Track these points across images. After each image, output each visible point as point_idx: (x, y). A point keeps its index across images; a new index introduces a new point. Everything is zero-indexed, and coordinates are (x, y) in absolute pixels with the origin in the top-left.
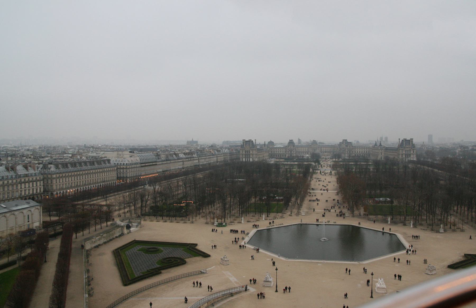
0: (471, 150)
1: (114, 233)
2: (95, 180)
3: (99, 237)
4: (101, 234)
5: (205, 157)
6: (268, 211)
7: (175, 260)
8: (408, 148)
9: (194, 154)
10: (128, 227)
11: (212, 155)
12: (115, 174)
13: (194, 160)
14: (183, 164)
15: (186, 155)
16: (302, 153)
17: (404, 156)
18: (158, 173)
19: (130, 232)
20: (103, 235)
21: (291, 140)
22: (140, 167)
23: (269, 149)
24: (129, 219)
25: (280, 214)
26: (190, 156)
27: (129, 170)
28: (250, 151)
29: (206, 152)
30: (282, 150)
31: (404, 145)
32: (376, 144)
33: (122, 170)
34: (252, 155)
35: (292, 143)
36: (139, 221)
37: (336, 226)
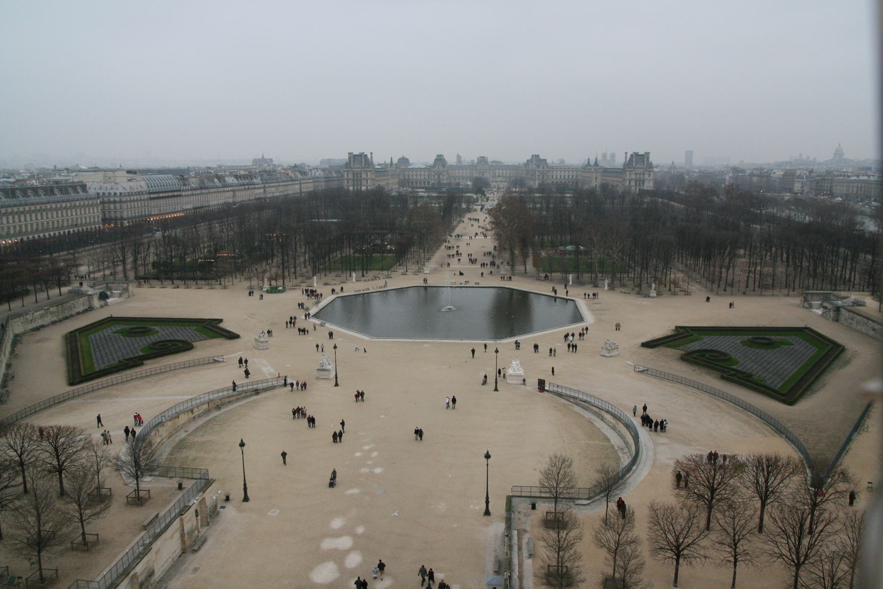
0: (749, 175)
1: (72, 306)
2: (58, 222)
3: (41, 312)
4: (45, 307)
5: (277, 184)
6: (363, 267)
7: (173, 345)
8: (640, 168)
9: (255, 177)
10: (103, 296)
11: (291, 181)
12: (98, 212)
13: (255, 188)
14: (234, 196)
15: (239, 179)
16: (464, 180)
17: (633, 183)
18: (184, 210)
19: (106, 305)
20: (49, 309)
21: (440, 156)
22: (147, 199)
23: (398, 170)
24: (107, 284)
25: (385, 273)
26: (247, 181)
27: (126, 204)
28: (361, 174)
29: (279, 175)
30: (422, 172)
31: (634, 164)
32: (589, 162)
33: (112, 206)
34: (365, 181)
35: (441, 160)
36: (125, 285)
37: (484, 289)
